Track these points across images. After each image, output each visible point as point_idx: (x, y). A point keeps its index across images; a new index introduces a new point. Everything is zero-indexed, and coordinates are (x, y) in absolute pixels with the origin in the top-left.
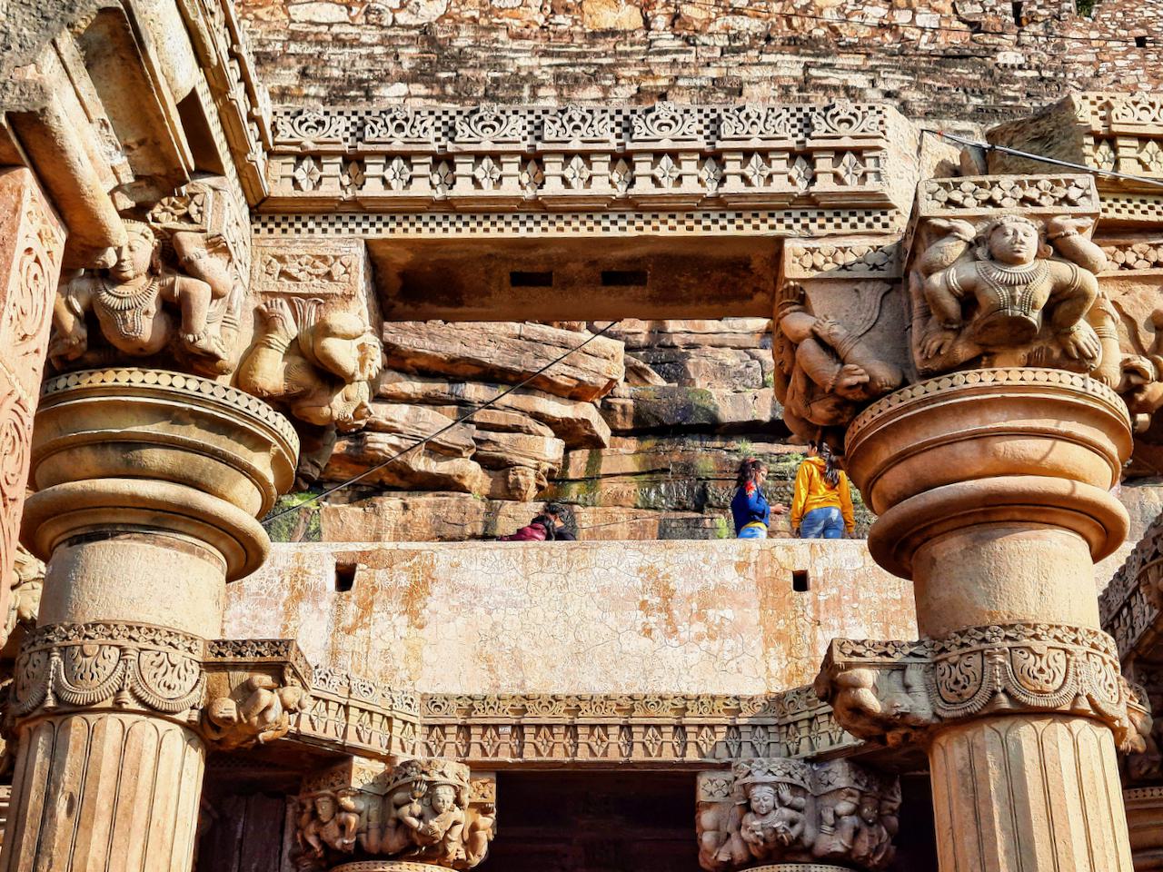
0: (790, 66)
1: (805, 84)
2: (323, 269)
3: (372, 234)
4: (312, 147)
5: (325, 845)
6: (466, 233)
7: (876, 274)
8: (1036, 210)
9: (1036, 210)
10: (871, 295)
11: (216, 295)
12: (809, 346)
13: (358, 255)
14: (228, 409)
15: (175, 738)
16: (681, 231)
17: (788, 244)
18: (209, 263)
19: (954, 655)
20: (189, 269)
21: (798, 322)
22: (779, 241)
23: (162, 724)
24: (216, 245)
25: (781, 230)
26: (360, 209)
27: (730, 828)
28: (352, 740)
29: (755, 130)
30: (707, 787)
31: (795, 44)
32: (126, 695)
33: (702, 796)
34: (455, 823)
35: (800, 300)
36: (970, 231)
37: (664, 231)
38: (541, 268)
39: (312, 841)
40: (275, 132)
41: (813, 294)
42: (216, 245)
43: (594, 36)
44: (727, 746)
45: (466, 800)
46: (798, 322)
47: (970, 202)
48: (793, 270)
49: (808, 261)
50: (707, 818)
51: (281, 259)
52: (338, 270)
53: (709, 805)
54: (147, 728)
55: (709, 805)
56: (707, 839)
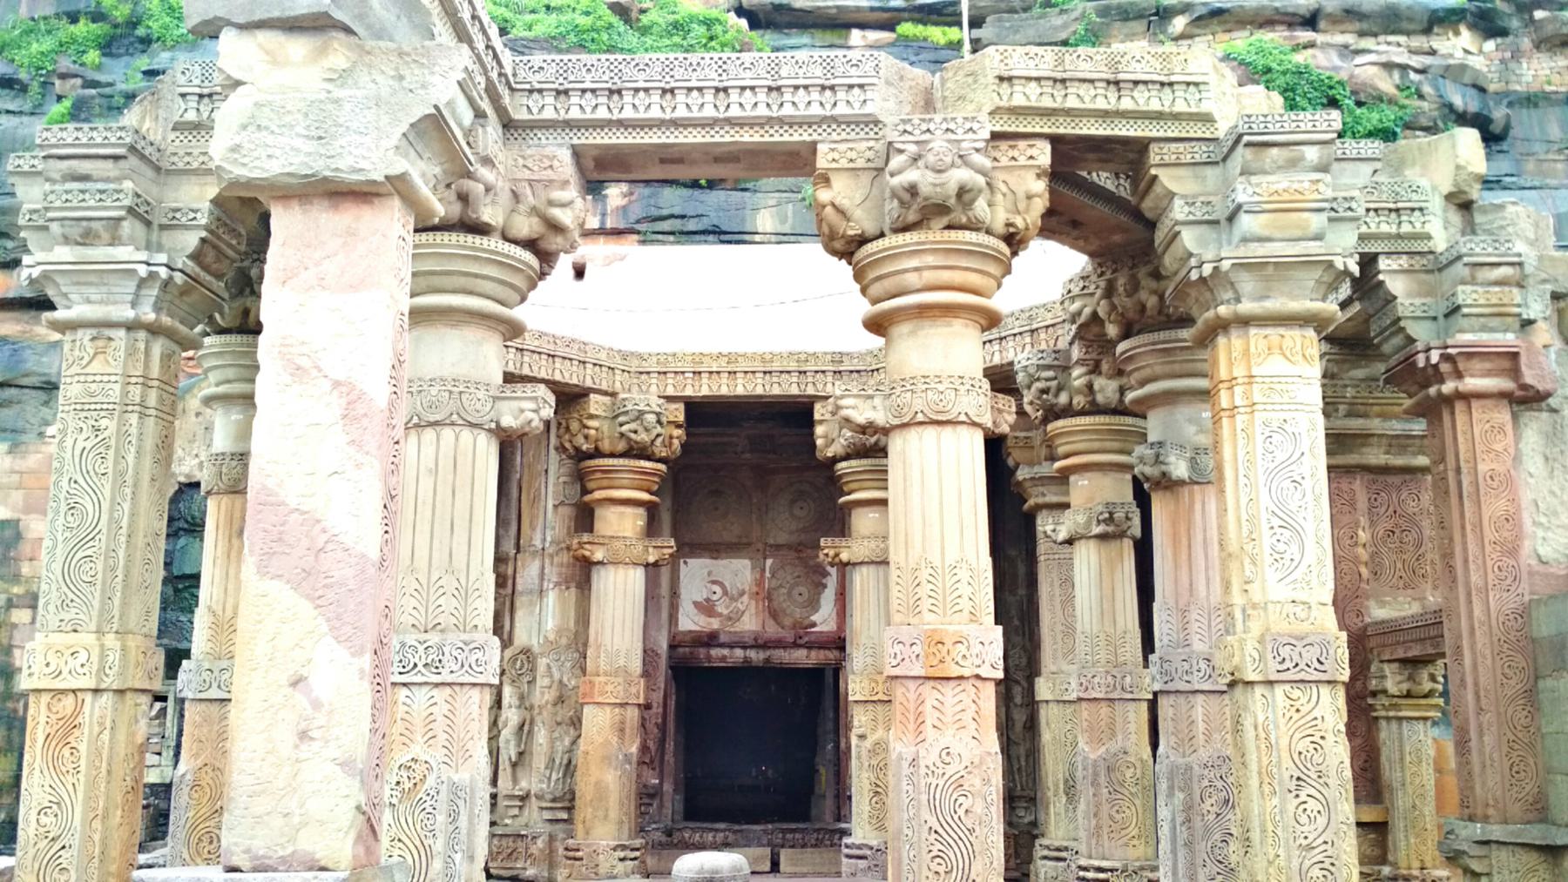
2: (547, 163)
3: (575, 141)
4: (538, 86)
5: (577, 449)
6: (630, 140)
7: (870, 165)
8: (953, 137)
9: (953, 137)
10: (866, 178)
11: (488, 190)
12: (829, 209)
13: (566, 155)
14: (498, 253)
15: (483, 438)
16: (757, 138)
17: (819, 146)
18: (484, 172)
19: (898, 391)
20: (469, 175)
21: (824, 195)
22: (815, 143)
23: (476, 431)
24: (487, 161)
25: (815, 137)
26: (569, 125)
27: (835, 435)
28: (589, 383)
29: (801, 72)
30: (819, 412)
32: (455, 417)
33: (817, 416)
34: (658, 435)
35: (825, 180)
36: (912, 148)
37: (746, 138)
38: (677, 156)
39: (567, 445)
40: (515, 75)
41: (834, 178)
42: (487, 161)
44: (498, 703)
45: (664, 420)
46: (824, 195)
47: (917, 132)
48: (822, 163)
49: (830, 157)
50: (819, 430)
51: (523, 157)
52: (556, 163)
53: (821, 422)
54: (466, 434)
55: (821, 422)
56: (819, 442)
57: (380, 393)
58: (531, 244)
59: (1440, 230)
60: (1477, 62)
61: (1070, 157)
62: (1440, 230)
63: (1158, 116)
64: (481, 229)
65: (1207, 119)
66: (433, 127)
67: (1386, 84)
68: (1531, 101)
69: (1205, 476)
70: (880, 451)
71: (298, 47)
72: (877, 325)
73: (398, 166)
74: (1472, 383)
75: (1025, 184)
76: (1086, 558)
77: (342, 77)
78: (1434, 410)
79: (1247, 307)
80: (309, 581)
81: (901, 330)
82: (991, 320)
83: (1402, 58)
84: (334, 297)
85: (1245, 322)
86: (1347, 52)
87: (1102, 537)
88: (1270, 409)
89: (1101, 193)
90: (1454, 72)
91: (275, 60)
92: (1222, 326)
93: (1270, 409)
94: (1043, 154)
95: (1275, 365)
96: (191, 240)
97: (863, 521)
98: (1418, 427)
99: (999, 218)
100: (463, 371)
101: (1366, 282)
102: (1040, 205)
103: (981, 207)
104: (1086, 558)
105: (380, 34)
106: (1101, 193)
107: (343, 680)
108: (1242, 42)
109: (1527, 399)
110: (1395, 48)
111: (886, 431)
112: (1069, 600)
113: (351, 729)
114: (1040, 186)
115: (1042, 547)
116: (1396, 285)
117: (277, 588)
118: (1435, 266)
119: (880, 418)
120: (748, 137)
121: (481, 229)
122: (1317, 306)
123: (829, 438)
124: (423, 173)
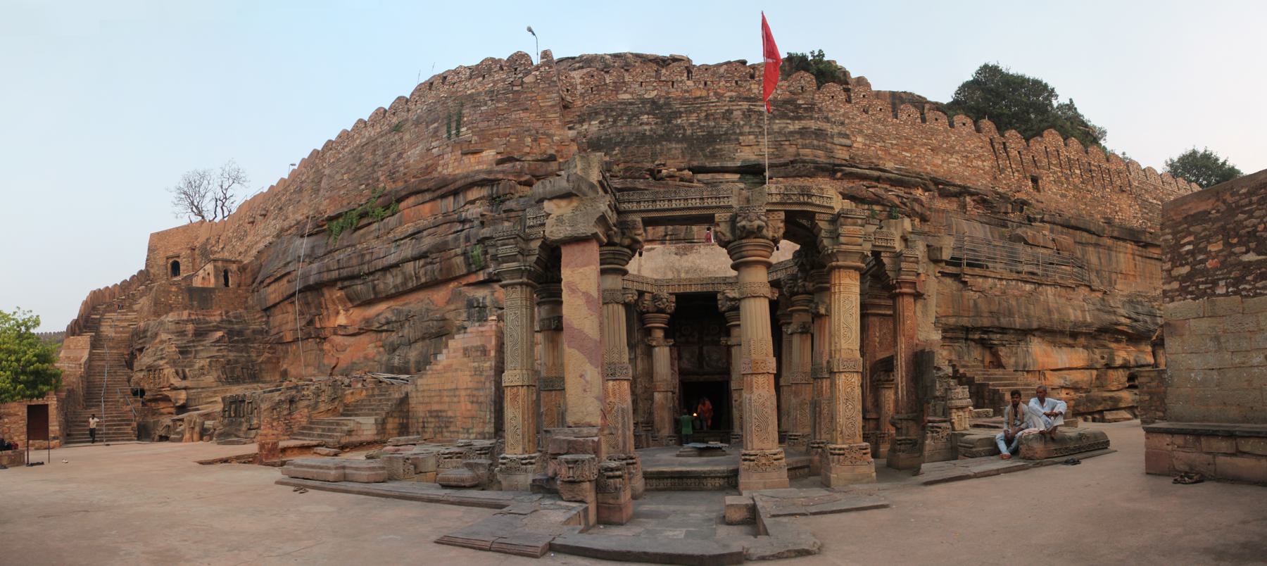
0: (745, 105)
1: (749, 110)
21: (718, 229)
30: (719, 296)
31: (747, 99)
43: (696, 98)
46: (718, 229)
57: (595, 294)
58: (628, 247)
59: (898, 246)
60: (923, 198)
61: (791, 218)
62: (898, 246)
63: (818, 206)
64: (614, 244)
65: (832, 208)
66: (602, 219)
67: (897, 201)
68: (937, 211)
69: (828, 314)
70: (737, 309)
71: (563, 203)
72: (734, 267)
73: (596, 230)
74: (904, 290)
75: (777, 224)
76: (796, 340)
77: (576, 209)
78: (894, 297)
79: (840, 263)
80: (581, 348)
81: (743, 269)
82: (769, 266)
83: (902, 194)
84: (581, 275)
85: (840, 267)
86: (887, 190)
87: (802, 333)
88: (847, 296)
89: (800, 225)
90: (917, 200)
91: (559, 207)
92: (834, 268)
93: (847, 296)
94: (782, 216)
95: (848, 281)
96: (534, 258)
97: (735, 332)
98: (890, 302)
99: (770, 234)
100: (613, 287)
101: (876, 254)
102: (782, 231)
103: (765, 231)
104: (796, 340)
105: (585, 195)
106: (800, 225)
107: (593, 374)
108: (847, 185)
109: (918, 296)
110: (901, 191)
111: (739, 300)
112: (791, 353)
113: (597, 389)
114: (782, 225)
115: (784, 336)
116: (886, 260)
117: (572, 350)
118: (898, 257)
119: (737, 295)
120: (694, 213)
121: (614, 244)
122: (859, 264)
123: (722, 305)
124: (600, 231)
